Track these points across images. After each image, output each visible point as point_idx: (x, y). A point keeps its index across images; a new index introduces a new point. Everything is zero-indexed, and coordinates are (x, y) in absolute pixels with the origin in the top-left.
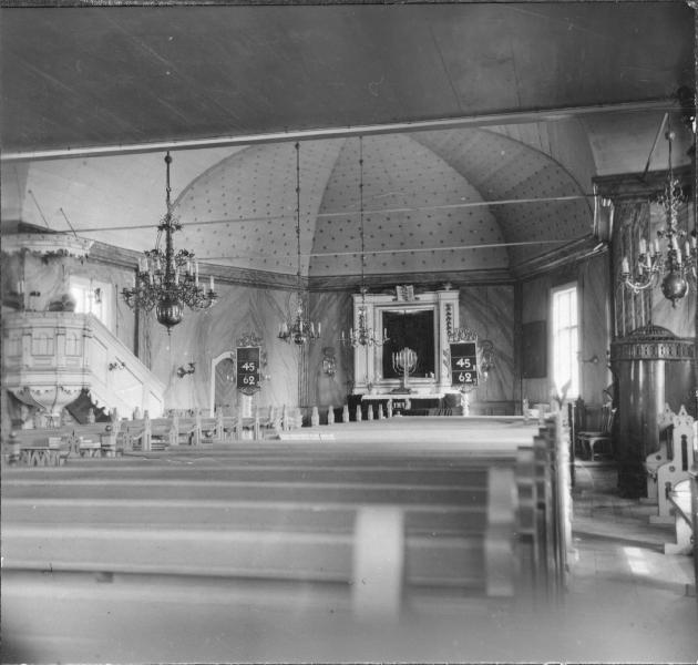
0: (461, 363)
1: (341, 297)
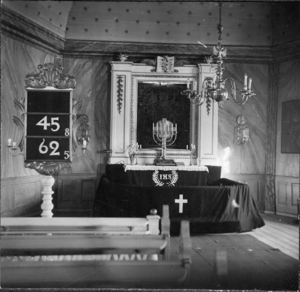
0: (44, 123)
1: (97, 64)
